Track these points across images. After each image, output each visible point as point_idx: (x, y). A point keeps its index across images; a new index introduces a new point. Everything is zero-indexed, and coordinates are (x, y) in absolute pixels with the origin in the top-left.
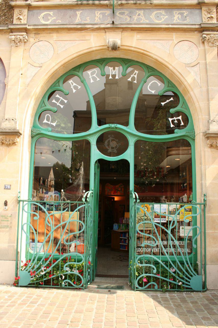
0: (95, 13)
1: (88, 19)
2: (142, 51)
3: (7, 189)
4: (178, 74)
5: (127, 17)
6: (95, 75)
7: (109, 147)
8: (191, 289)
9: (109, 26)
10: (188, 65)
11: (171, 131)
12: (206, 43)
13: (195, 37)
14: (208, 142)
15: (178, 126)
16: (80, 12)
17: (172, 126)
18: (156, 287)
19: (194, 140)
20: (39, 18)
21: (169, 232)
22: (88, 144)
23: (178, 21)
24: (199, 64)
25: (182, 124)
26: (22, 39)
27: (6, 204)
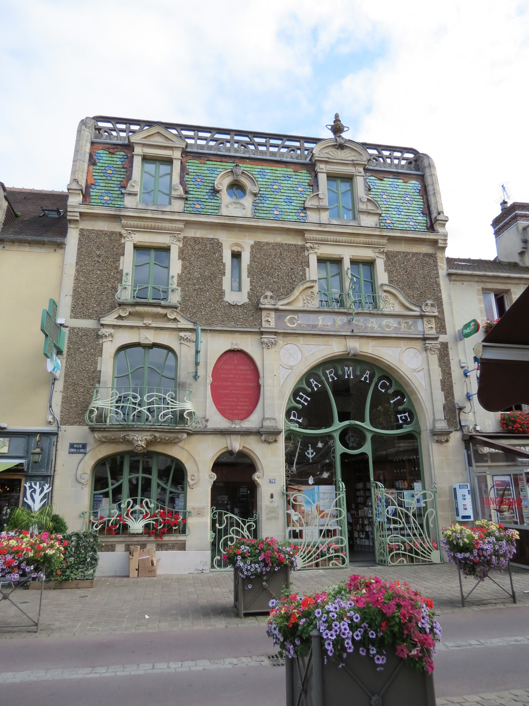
3: (272, 482)
7: (350, 442)
8: (432, 562)
9: (349, 334)
10: (414, 370)
11: (400, 427)
12: (428, 351)
13: (419, 345)
15: (405, 421)
16: (321, 318)
18: (405, 562)
19: (420, 434)
20: (286, 320)
21: (411, 514)
23: (405, 330)
24: (423, 370)
25: (409, 420)
26: (274, 342)
27: (272, 496)
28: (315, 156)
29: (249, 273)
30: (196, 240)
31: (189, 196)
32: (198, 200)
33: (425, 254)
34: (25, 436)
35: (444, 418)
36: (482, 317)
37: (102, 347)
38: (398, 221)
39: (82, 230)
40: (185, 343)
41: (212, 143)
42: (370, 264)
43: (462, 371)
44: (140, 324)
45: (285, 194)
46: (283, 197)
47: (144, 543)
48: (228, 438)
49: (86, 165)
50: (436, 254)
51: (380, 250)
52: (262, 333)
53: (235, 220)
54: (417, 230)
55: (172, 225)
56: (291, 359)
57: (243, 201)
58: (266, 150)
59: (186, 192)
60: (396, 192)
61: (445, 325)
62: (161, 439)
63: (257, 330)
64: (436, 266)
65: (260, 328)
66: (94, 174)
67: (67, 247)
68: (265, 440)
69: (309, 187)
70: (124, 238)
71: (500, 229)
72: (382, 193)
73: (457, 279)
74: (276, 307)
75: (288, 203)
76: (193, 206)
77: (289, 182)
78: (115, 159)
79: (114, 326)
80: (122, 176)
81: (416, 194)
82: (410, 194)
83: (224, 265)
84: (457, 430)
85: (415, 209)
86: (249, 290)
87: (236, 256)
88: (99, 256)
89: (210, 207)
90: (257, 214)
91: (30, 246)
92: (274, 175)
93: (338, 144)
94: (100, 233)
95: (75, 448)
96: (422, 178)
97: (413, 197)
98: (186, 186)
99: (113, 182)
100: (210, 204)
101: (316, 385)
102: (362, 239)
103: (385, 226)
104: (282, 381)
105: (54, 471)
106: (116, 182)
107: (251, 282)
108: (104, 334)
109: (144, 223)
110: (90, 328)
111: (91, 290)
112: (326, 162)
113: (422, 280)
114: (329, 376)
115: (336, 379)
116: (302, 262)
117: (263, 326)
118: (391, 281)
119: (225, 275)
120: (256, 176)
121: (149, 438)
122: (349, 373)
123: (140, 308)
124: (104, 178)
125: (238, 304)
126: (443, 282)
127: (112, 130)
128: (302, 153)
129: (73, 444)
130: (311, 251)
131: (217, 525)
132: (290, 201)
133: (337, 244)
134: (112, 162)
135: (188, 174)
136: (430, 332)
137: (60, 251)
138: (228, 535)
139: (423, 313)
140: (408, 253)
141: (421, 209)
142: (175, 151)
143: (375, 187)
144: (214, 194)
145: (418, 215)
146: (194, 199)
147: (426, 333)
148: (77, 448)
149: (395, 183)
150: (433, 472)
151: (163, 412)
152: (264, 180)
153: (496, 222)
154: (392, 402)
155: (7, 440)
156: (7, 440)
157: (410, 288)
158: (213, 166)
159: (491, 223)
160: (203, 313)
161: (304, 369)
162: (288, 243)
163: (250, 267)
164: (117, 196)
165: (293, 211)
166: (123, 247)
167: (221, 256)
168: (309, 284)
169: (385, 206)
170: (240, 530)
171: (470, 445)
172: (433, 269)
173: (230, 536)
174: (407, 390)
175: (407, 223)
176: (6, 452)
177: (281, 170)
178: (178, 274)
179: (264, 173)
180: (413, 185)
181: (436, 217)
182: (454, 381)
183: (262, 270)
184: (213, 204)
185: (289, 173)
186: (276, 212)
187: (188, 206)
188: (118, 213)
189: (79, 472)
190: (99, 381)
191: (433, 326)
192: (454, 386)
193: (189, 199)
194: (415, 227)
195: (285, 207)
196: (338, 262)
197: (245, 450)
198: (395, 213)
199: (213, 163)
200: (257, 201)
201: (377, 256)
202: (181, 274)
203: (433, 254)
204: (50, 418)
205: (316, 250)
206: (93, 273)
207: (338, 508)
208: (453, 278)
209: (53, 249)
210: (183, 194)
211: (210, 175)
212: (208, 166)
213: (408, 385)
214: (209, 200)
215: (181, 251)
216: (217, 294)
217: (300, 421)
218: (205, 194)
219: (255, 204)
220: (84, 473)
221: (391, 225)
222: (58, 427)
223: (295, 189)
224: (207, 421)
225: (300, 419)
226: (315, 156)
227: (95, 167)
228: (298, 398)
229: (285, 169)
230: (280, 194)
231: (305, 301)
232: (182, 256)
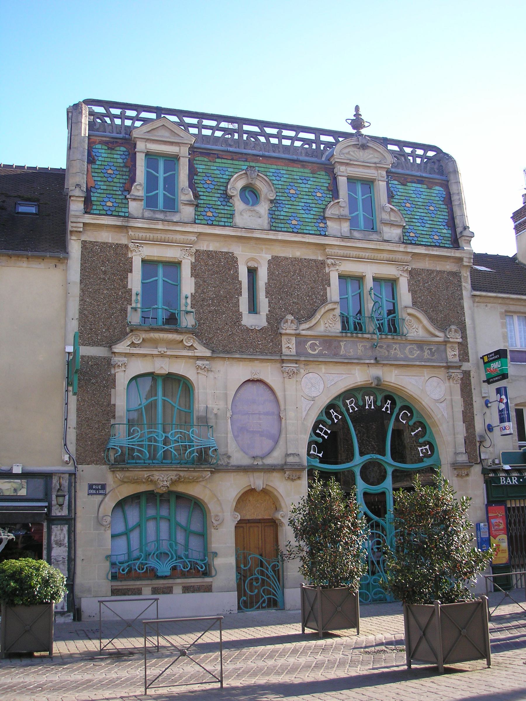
0: (357, 345)
1: (351, 352)
2: (400, 387)
4: (429, 410)
5: (385, 351)
6: (353, 405)
10: (437, 401)
11: (421, 460)
12: (451, 380)
14: (455, 472)
15: (426, 456)
17: (421, 455)
22: (353, 474)
23: (428, 357)
28: (335, 157)
29: (267, 293)
30: (209, 254)
31: (200, 201)
32: (210, 207)
33: (449, 272)
34: (42, 477)
35: (465, 452)
36: (504, 342)
37: (115, 379)
38: (422, 234)
39: (84, 243)
40: (203, 373)
41: (219, 134)
42: (393, 282)
43: (483, 401)
44: (155, 352)
45: (303, 200)
46: (300, 204)
47: (170, 585)
48: (250, 474)
49: (86, 163)
50: (460, 273)
52: (283, 361)
53: (252, 233)
54: (441, 245)
55: (183, 237)
56: (313, 389)
57: (257, 208)
58: (277, 143)
59: (196, 196)
60: (420, 200)
62: (185, 478)
63: (278, 358)
64: (460, 286)
65: (281, 356)
66: (94, 174)
67: (70, 262)
68: (288, 478)
69: (328, 192)
70: (131, 251)
71: (520, 224)
72: (405, 201)
73: (481, 300)
74: (298, 332)
75: (307, 212)
76: (204, 213)
77: (307, 186)
78: (115, 156)
79: (126, 355)
80: (124, 177)
81: (441, 202)
82: (435, 202)
83: (240, 283)
84: (477, 464)
85: (440, 220)
86: (268, 313)
87: (252, 272)
88: (105, 273)
89: (223, 215)
90: (274, 224)
91: (29, 261)
92: (291, 177)
93: (360, 144)
94: (105, 246)
95: (94, 489)
96: (446, 185)
97: (437, 206)
98: (195, 190)
99: (115, 184)
100: (222, 211)
101: (335, 416)
102: (385, 256)
103: (409, 240)
104: (304, 414)
105: (75, 514)
106: (118, 185)
107: (269, 303)
108: (117, 364)
109: (154, 235)
110: (100, 357)
111: (99, 312)
112: (347, 164)
113: (446, 302)
114: (349, 406)
115: (356, 409)
116: (322, 280)
117: (284, 353)
118: (414, 303)
119: (241, 294)
120: (271, 178)
121: (174, 478)
122: (369, 403)
123: (154, 334)
124: (105, 179)
125: (257, 328)
126: (467, 303)
127: (104, 115)
128: (318, 147)
130: (332, 268)
131: (242, 566)
132: (309, 208)
133: (359, 259)
134: (112, 160)
135: (197, 175)
136: (453, 360)
137: (61, 267)
138: (253, 575)
139: (447, 339)
140: (433, 271)
141: (446, 221)
142: (182, 148)
143: (399, 194)
144: (226, 200)
145: (442, 227)
146: (205, 206)
147: (449, 360)
148: (96, 489)
149: (418, 189)
151: (189, 450)
152: (280, 183)
153: (516, 216)
154: (413, 434)
155: (25, 482)
156: (25, 482)
157: (433, 310)
158: (223, 165)
159: (512, 215)
160: (220, 339)
161: (325, 401)
162: (307, 258)
163: (268, 285)
164: (120, 201)
165: (313, 220)
166: (130, 262)
167: (237, 272)
168: (330, 306)
169: (409, 216)
172: (458, 289)
173: (256, 576)
174: (428, 421)
175: (432, 237)
176: (25, 494)
177: (298, 172)
178: (192, 294)
179: (280, 175)
180: (437, 192)
181: (461, 232)
182: (475, 413)
183: (281, 289)
184: (226, 212)
185: (306, 175)
186: (294, 222)
187: (199, 213)
188: (126, 224)
189: (101, 515)
190: (114, 416)
191: (457, 353)
192: (476, 417)
193: (199, 205)
194: (439, 241)
195: (304, 216)
196: (360, 279)
197: (268, 488)
198: (419, 225)
199: (223, 161)
200: (274, 209)
201: (401, 275)
202: (195, 293)
203: (457, 273)
204: (66, 458)
205: (337, 267)
206: (99, 293)
208: (477, 299)
209: (53, 265)
210: (193, 199)
211: (221, 176)
212: (218, 165)
213: (430, 417)
214: (222, 207)
215: (194, 267)
216: (234, 317)
217: (321, 455)
218: (216, 199)
219: (271, 212)
220: (106, 515)
221: (415, 239)
222: (75, 467)
223: (314, 194)
224: (229, 457)
225: (320, 453)
226: (335, 157)
227: (93, 166)
228: (318, 431)
229: (302, 170)
230: (297, 200)
231: (327, 325)
232: (195, 273)
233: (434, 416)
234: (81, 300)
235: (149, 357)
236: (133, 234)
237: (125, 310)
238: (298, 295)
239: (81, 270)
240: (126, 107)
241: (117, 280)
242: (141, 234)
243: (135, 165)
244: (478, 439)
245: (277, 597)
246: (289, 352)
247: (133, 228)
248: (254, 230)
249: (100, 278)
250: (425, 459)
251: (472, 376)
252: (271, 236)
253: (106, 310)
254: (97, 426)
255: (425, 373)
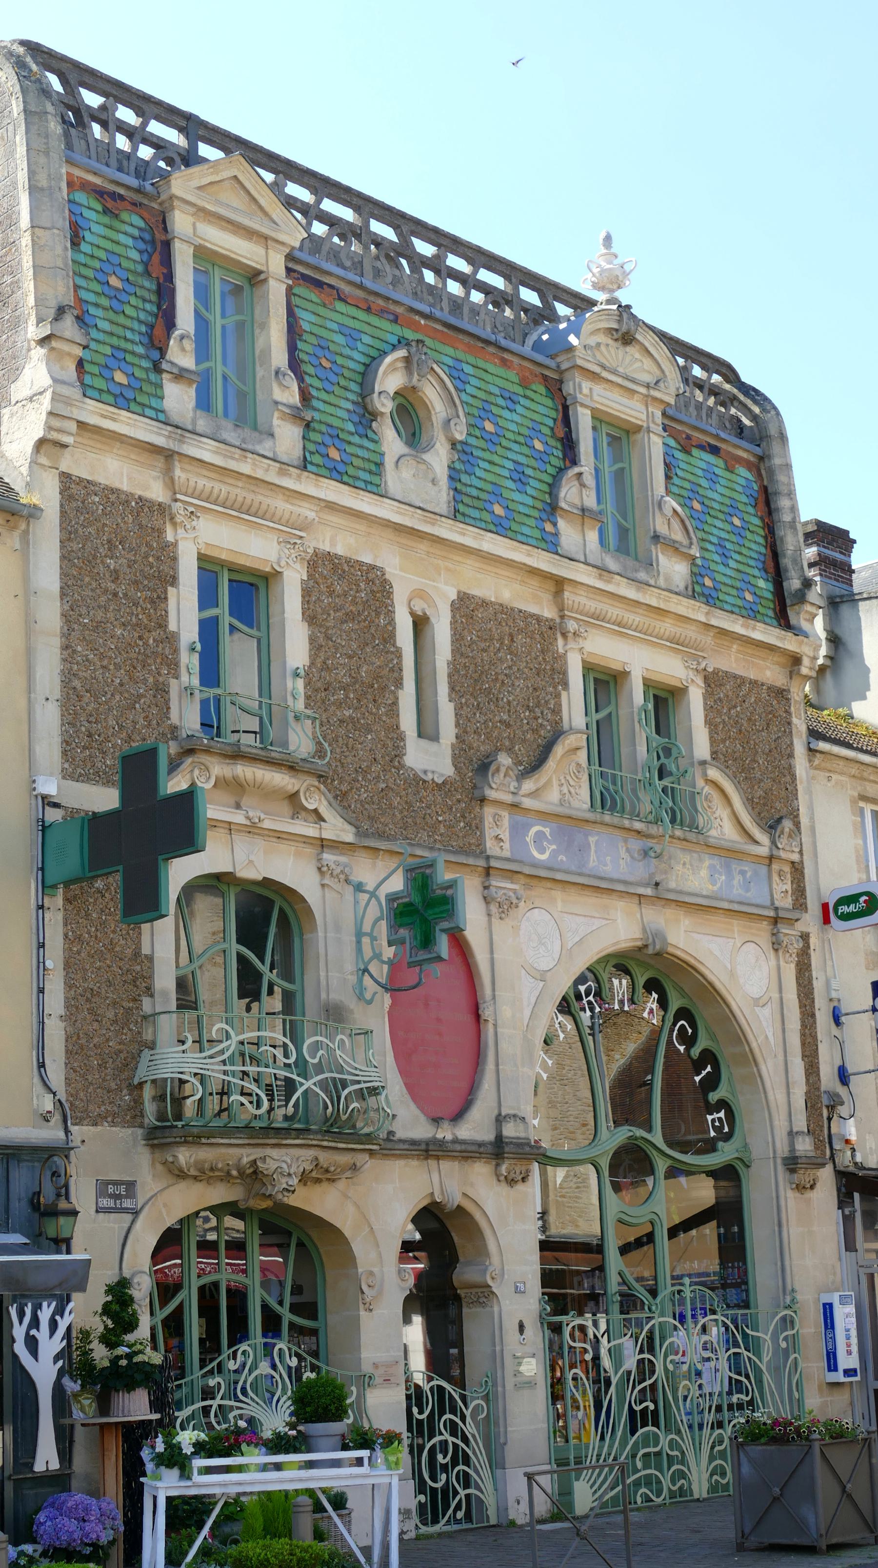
10: (756, 1002)
12: (781, 952)
27: (521, 1327)
44: (239, 818)
50: (789, 691)
51: (699, 663)
59: (305, 397)
61: (805, 887)
74: (517, 799)
87: (420, 624)
88: (115, 576)
104: (527, 1013)
118: (714, 754)
123: (246, 769)
129: (107, 1183)
131: (415, 1410)
148: (116, 1197)
150: (787, 1263)
154: (697, 1079)
162: (523, 608)
170: (458, 1420)
171: (852, 1198)
201: (692, 680)
202: (309, 667)
207: (646, 1356)
233: (750, 1037)
234: (65, 647)
235: (222, 830)
236: (183, 476)
237: (162, 690)
238: (509, 702)
239: (63, 558)
240: (125, 96)
241: (144, 601)
242: (203, 483)
243: (170, 277)
244: (825, 1100)
245: (482, 1492)
246: (498, 849)
247: (186, 460)
248: (438, 517)
249: (106, 591)
250: (720, 1144)
251: (812, 947)
252: (447, 530)
253: (121, 685)
254: (110, 1014)
255: (736, 929)
